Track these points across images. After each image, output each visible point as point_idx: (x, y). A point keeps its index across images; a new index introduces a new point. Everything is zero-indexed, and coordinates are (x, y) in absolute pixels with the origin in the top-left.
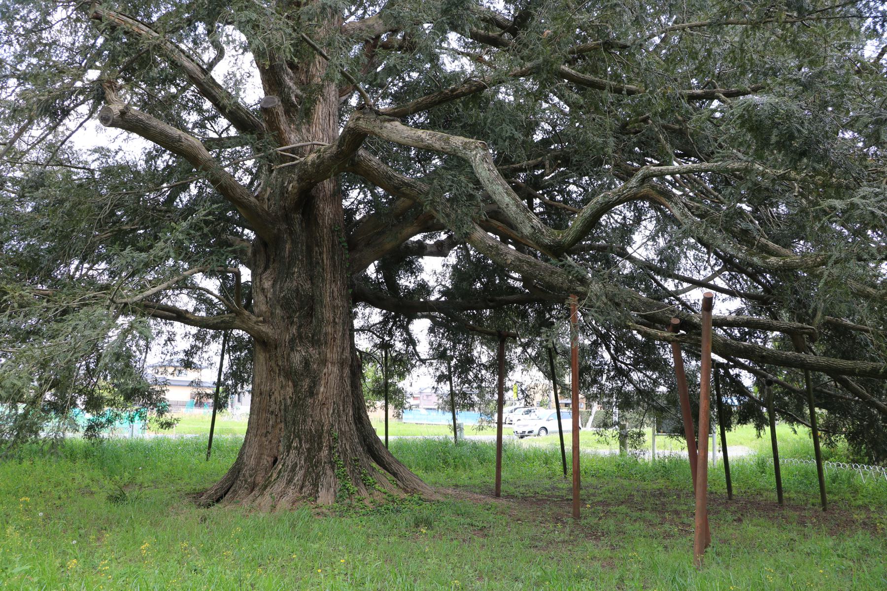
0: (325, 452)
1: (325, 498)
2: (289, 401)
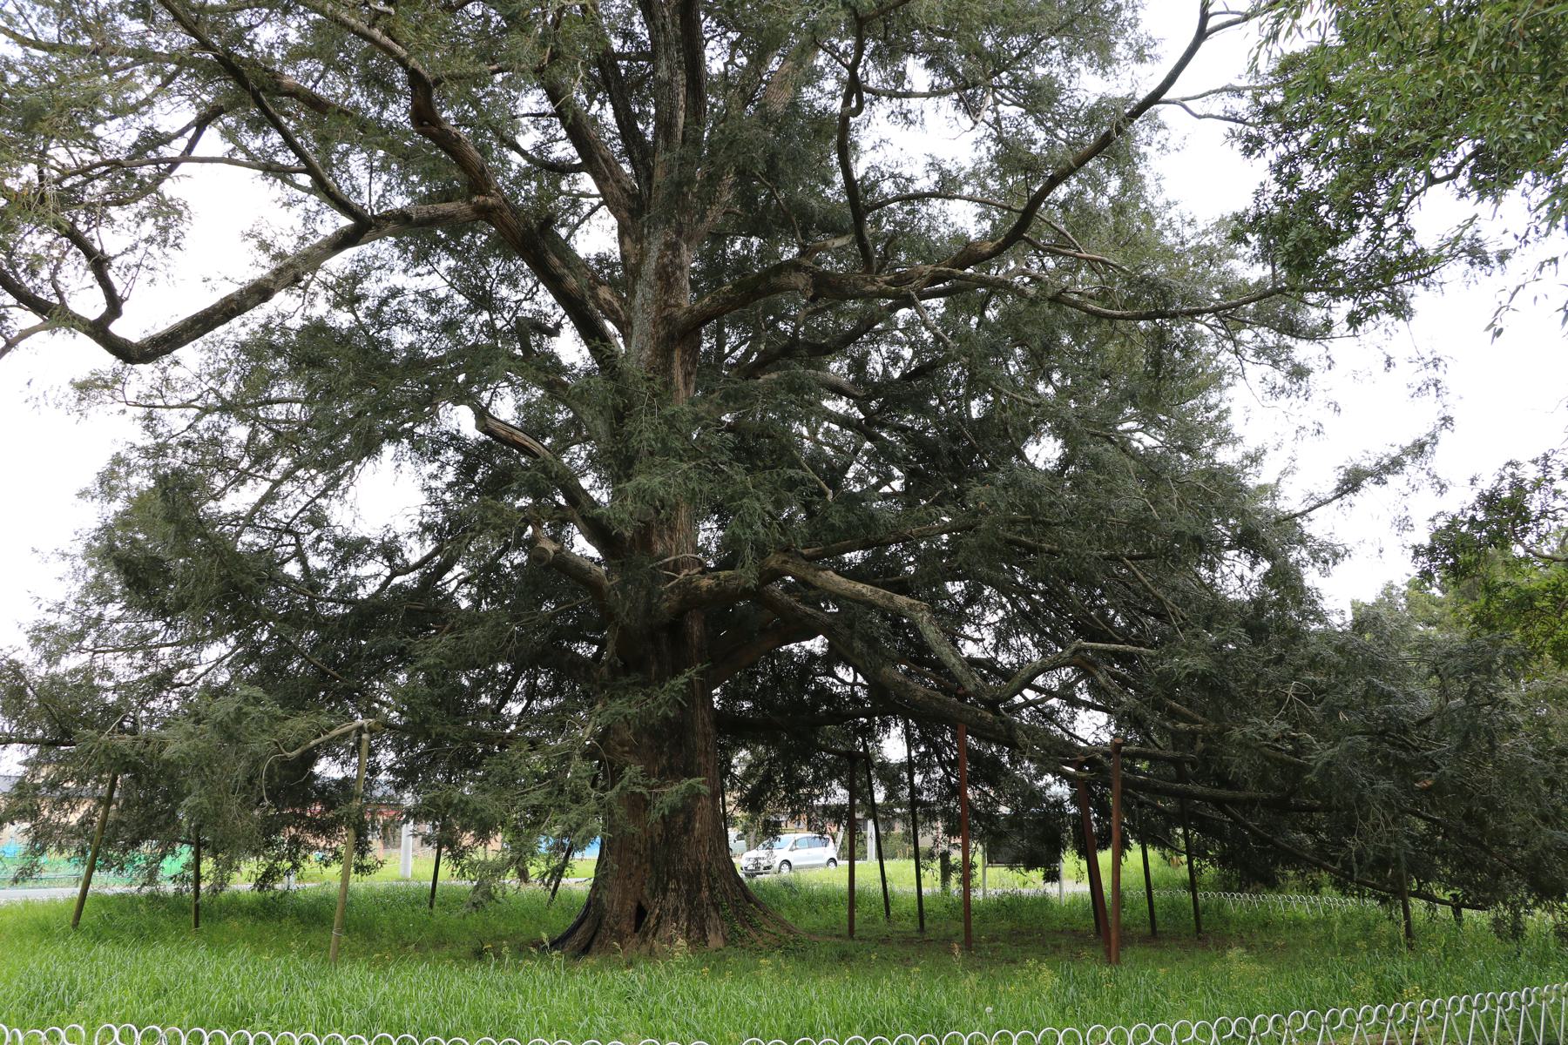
0: (705, 894)
1: (715, 941)
2: (657, 840)
